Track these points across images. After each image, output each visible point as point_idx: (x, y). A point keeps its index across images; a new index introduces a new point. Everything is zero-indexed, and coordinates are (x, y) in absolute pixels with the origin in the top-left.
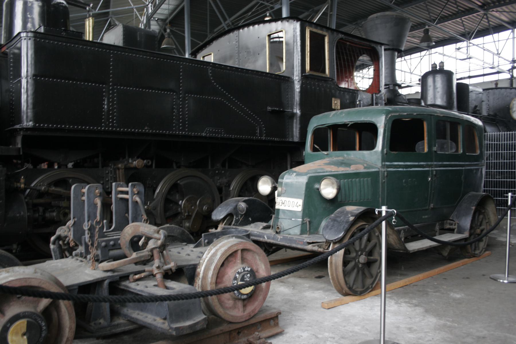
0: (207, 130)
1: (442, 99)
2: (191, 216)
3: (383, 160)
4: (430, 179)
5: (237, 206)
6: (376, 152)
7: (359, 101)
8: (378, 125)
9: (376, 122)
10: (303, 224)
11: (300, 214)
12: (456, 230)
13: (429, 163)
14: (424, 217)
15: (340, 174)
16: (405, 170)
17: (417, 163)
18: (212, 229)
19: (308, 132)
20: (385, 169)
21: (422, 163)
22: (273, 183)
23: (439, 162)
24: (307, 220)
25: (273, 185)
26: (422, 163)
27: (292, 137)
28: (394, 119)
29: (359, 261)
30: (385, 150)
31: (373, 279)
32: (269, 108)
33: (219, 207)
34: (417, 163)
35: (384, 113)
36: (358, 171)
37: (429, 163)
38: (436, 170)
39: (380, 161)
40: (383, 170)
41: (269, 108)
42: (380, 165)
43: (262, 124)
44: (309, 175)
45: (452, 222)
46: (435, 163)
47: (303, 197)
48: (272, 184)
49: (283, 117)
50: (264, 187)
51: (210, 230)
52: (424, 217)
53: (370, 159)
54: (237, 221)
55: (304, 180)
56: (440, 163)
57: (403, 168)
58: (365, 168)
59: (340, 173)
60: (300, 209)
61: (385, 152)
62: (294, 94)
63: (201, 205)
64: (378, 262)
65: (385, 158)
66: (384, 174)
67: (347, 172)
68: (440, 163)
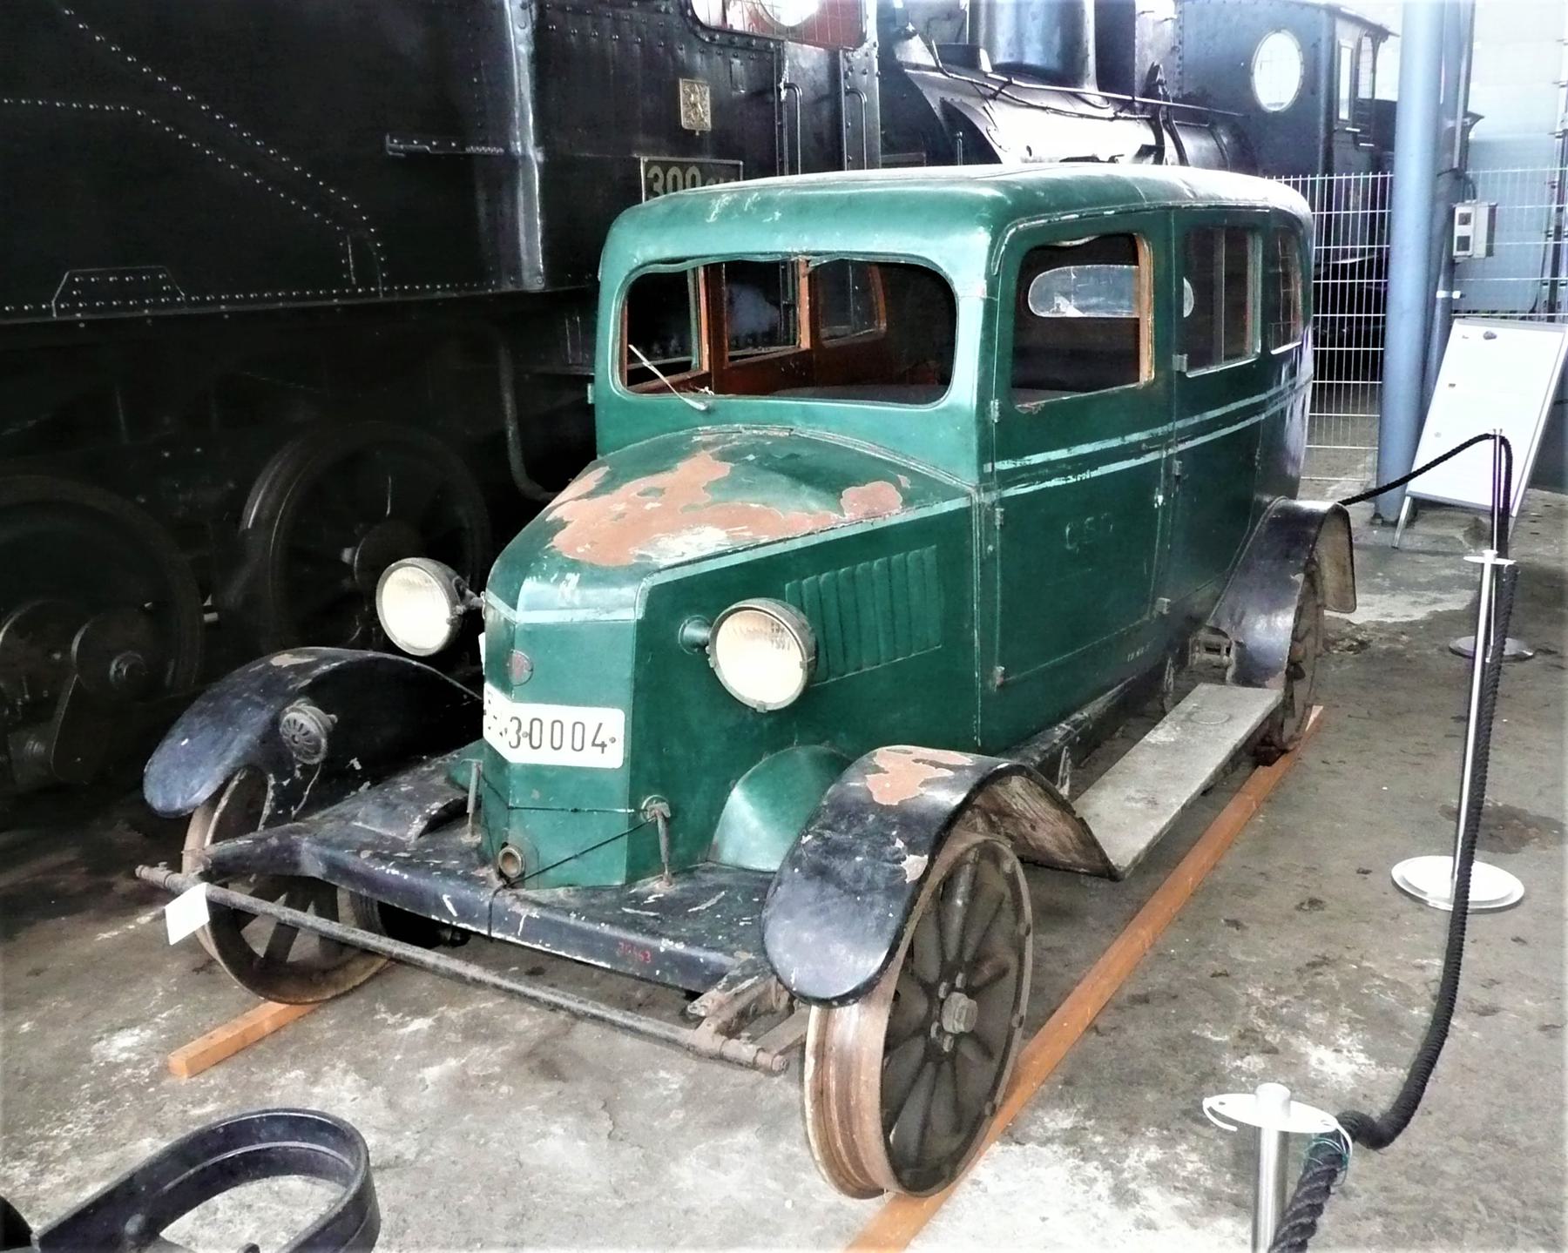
0: (71, 284)
1: (1047, 43)
2: (53, 702)
3: (987, 452)
4: (1160, 499)
5: (275, 722)
6: (951, 411)
7: (787, 86)
8: (958, 288)
9: (946, 269)
10: (638, 829)
11: (621, 787)
12: (1230, 673)
13: (1159, 431)
14: (1131, 656)
15: (799, 553)
16: (1072, 480)
17: (1115, 443)
18: (154, 865)
19: (604, 290)
20: (994, 496)
21: (1135, 437)
22: (458, 595)
23: (1192, 415)
24: (655, 808)
25: (461, 609)
26: (1135, 437)
27: (516, 270)
28: (1026, 245)
29: (941, 1030)
30: (995, 404)
31: (995, 1065)
32: (393, 144)
33: (178, 731)
34: (1115, 443)
35: (983, 222)
36: (880, 524)
37: (1159, 431)
38: (1180, 455)
39: (973, 458)
40: (987, 499)
41: (393, 144)
42: (975, 480)
43: (368, 224)
44: (648, 583)
45: (1215, 639)
46: (1180, 424)
47: (625, 692)
48: (453, 604)
49: (462, 184)
50: (414, 608)
51: (144, 872)
52: (1131, 656)
53: (928, 450)
54: (287, 799)
55: (625, 606)
56: (1196, 419)
57: (1064, 474)
58: (908, 501)
59: (798, 544)
60: (614, 757)
61: (995, 416)
62: (508, 67)
63: (94, 655)
64: (1013, 974)
65: (1000, 439)
66: (989, 518)
67: (832, 536)
68: (1196, 419)
